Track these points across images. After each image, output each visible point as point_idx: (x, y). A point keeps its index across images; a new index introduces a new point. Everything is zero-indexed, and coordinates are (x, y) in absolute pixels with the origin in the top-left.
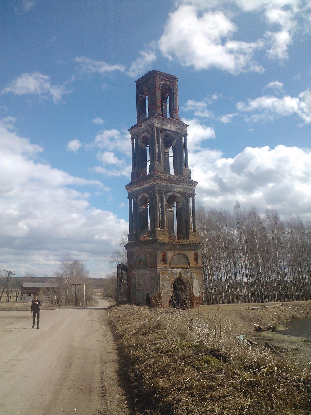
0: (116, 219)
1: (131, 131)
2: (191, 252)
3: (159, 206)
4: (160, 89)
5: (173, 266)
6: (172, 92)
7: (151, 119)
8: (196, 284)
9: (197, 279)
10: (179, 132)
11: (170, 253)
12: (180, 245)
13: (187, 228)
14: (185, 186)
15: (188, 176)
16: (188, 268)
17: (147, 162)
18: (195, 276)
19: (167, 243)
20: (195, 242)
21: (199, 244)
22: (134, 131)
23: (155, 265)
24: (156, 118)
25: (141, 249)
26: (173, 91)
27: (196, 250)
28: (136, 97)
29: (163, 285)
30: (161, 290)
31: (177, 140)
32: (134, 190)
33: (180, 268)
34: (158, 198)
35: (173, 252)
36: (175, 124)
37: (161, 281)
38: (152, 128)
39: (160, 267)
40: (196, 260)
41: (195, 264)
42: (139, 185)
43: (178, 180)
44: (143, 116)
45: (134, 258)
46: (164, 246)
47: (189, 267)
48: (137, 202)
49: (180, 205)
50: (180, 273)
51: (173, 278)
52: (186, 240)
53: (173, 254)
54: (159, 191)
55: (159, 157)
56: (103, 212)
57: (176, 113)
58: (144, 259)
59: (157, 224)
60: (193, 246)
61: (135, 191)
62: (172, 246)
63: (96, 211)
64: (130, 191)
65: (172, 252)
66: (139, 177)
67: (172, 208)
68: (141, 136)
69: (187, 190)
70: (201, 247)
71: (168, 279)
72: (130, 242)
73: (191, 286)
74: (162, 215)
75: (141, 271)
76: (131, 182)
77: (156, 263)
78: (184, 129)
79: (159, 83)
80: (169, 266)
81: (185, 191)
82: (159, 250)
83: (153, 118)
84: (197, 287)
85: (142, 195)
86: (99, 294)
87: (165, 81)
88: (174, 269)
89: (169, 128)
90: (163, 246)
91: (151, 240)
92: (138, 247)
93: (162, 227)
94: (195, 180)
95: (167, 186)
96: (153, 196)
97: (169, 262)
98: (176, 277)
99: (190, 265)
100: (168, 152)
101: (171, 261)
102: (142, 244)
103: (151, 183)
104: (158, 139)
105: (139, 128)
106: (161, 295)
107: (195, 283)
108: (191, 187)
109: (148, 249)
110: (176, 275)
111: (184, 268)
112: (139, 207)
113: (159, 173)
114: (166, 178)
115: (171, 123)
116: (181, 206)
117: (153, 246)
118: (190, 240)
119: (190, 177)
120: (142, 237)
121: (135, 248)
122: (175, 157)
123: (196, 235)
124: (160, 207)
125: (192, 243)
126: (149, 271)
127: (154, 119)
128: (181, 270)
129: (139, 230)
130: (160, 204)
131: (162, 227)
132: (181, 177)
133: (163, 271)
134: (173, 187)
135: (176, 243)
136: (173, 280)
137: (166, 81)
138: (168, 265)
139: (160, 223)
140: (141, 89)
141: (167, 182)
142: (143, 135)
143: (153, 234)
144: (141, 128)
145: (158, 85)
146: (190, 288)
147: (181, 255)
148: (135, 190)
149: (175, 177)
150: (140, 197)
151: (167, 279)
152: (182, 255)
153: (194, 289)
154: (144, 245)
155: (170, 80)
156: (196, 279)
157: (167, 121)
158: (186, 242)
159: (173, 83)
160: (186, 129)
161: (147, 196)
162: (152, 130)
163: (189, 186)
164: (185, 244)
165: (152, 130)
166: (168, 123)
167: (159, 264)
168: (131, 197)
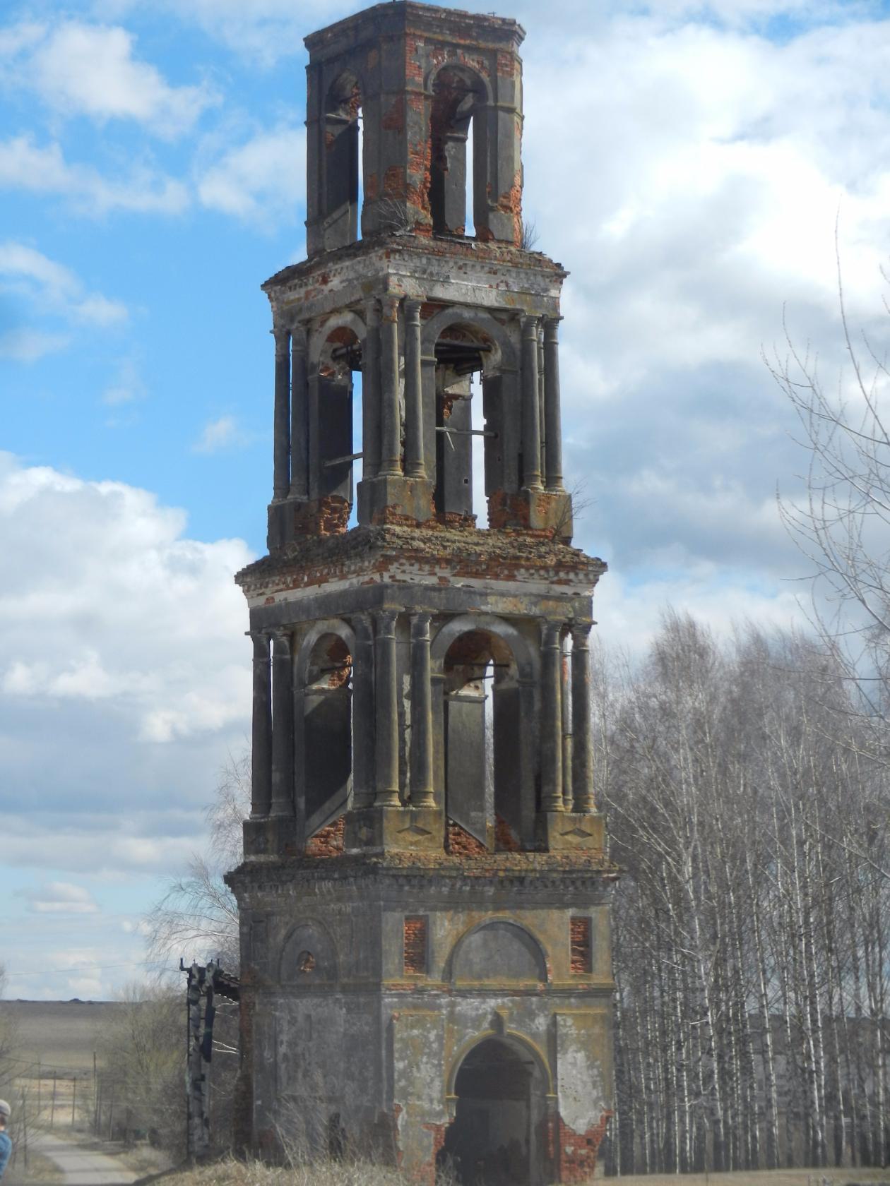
0: (177, 540)
1: (273, 295)
2: (555, 914)
3: (400, 689)
4: (427, 97)
5: (460, 984)
6: (491, 103)
7: (373, 255)
8: (574, 1072)
9: (584, 1045)
10: (518, 310)
11: (446, 923)
12: (501, 882)
13: (543, 795)
14: (537, 586)
15: (558, 532)
16: (536, 995)
18: (573, 1031)
19: (431, 873)
20: (577, 867)
21: (599, 872)
22: (292, 295)
23: (371, 980)
24: (399, 251)
26: (496, 99)
27: (584, 903)
29: (405, 1074)
30: (396, 1101)
31: (506, 345)
32: (280, 597)
33: (495, 993)
34: (396, 651)
35: (462, 917)
36: (495, 273)
37: (396, 1055)
38: (379, 301)
39: (393, 992)
40: (582, 954)
41: (572, 972)
42: (306, 579)
43: (504, 558)
44: (335, 221)
45: (271, 940)
46: (421, 887)
47: (540, 986)
48: (296, 659)
49: (512, 678)
50: (498, 1022)
51: (459, 1040)
52: (531, 855)
53: (461, 928)
54: (405, 620)
55: (410, 444)
56: (71, 485)
58: (319, 947)
59: (388, 781)
60: (568, 882)
61: (288, 604)
62: (458, 886)
63: (15, 479)
64: (261, 601)
65: (460, 915)
66: (309, 537)
67: (478, 683)
68: (323, 323)
69: (551, 603)
70: (609, 889)
71: (435, 1046)
72: (253, 858)
73: (549, 1081)
74: (413, 734)
75: (305, 1006)
77: (377, 971)
78: (546, 290)
79: (419, 67)
80: (440, 983)
81: (535, 611)
82: (394, 910)
83: (381, 252)
84: (579, 1082)
85: (322, 626)
86: (64, 1117)
87: (453, 54)
88: (464, 996)
89: (466, 294)
90: (412, 886)
91: (355, 859)
92: (291, 887)
93: (414, 796)
94: (590, 551)
95: (443, 592)
96: (370, 643)
97: (442, 965)
98: (473, 1035)
99: (550, 977)
100: (466, 394)
101: (450, 963)
102: (313, 878)
103: (366, 578)
104: (408, 351)
106: (396, 1125)
107: (570, 1067)
108: (569, 590)
109: (339, 899)
111: (516, 993)
112: (305, 686)
113: (405, 528)
114: (439, 553)
115: (478, 268)
116: (515, 685)
117: (363, 886)
118: (552, 853)
119: (567, 535)
120: (316, 836)
121: (277, 891)
122: (496, 436)
123: (589, 832)
124: (407, 697)
125: (564, 872)
126: (344, 1010)
127: (388, 257)
128: (499, 1001)
129: (301, 802)
130: (407, 679)
131: (412, 792)
132: (521, 539)
133: (408, 1008)
134: (474, 593)
135: (477, 872)
136: (458, 1050)
137: (459, 51)
138: (435, 979)
139: (402, 773)
140: (334, 82)
141: (445, 572)
142: (334, 322)
143: (364, 830)
144: (324, 287)
145: (417, 78)
146: (547, 1089)
147: (501, 932)
148: (286, 599)
149: (490, 541)
150: (311, 638)
151: (430, 1047)
152: (511, 927)
153: (566, 1097)
154: (324, 879)
155: (482, 44)
156: (573, 1048)
157: (456, 263)
158: (531, 867)
159: (496, 56)
160: (553, 293)
161: (347, 636)
162: (378, 311)
163: (560, 582)
164: (523, 874)
165: (378, 311)
166: (460, 268)
167: (392, 976)
168: (263, 632)
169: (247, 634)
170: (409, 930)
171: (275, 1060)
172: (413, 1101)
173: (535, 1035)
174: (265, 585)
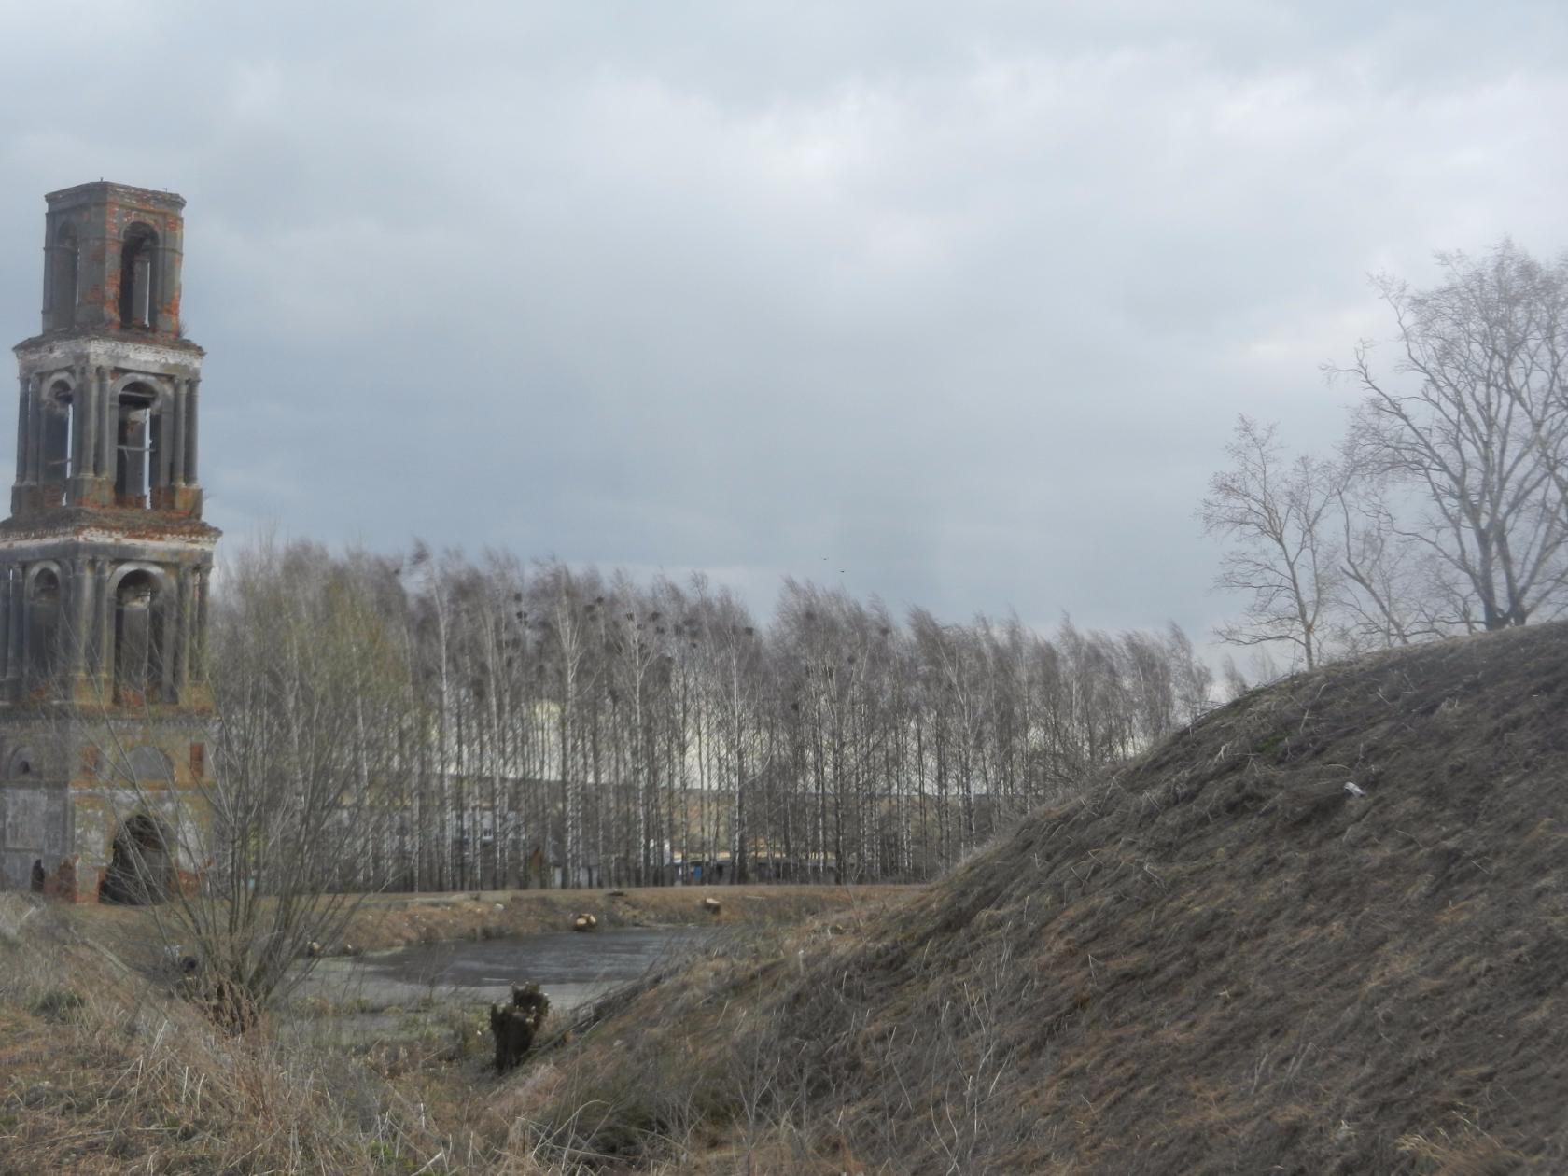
25: (26, 731)
37: (77, 820)
57: (169, 311)
75: (23, 794)
93: (93, 668)
105: (44, 351)
141: (119, 536)
142: (57, 377)
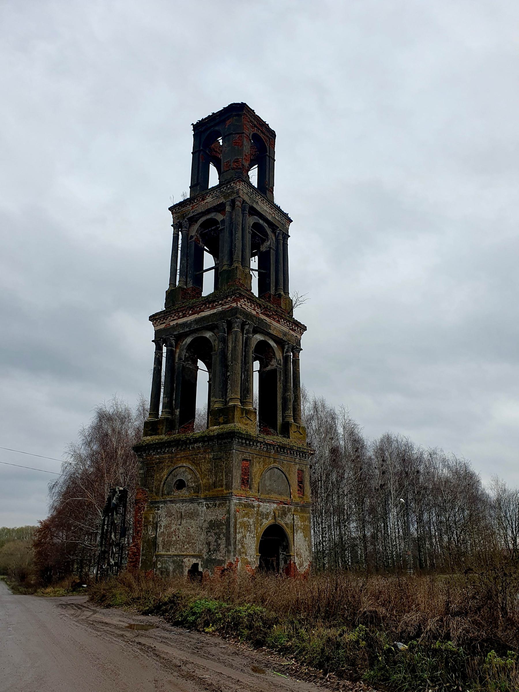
17: (214, 265)
28: (215, 112)
76: (165, 309)
98: (267, 523)
110: (267, 519)
136: (261, 530)
141: (259, 311)
163: (292, 330)
169: (153, 341)
170: (243, 466)
171: (156, 536)
172: (243, 555)
173: (287, 524)
174: (166, 318)
